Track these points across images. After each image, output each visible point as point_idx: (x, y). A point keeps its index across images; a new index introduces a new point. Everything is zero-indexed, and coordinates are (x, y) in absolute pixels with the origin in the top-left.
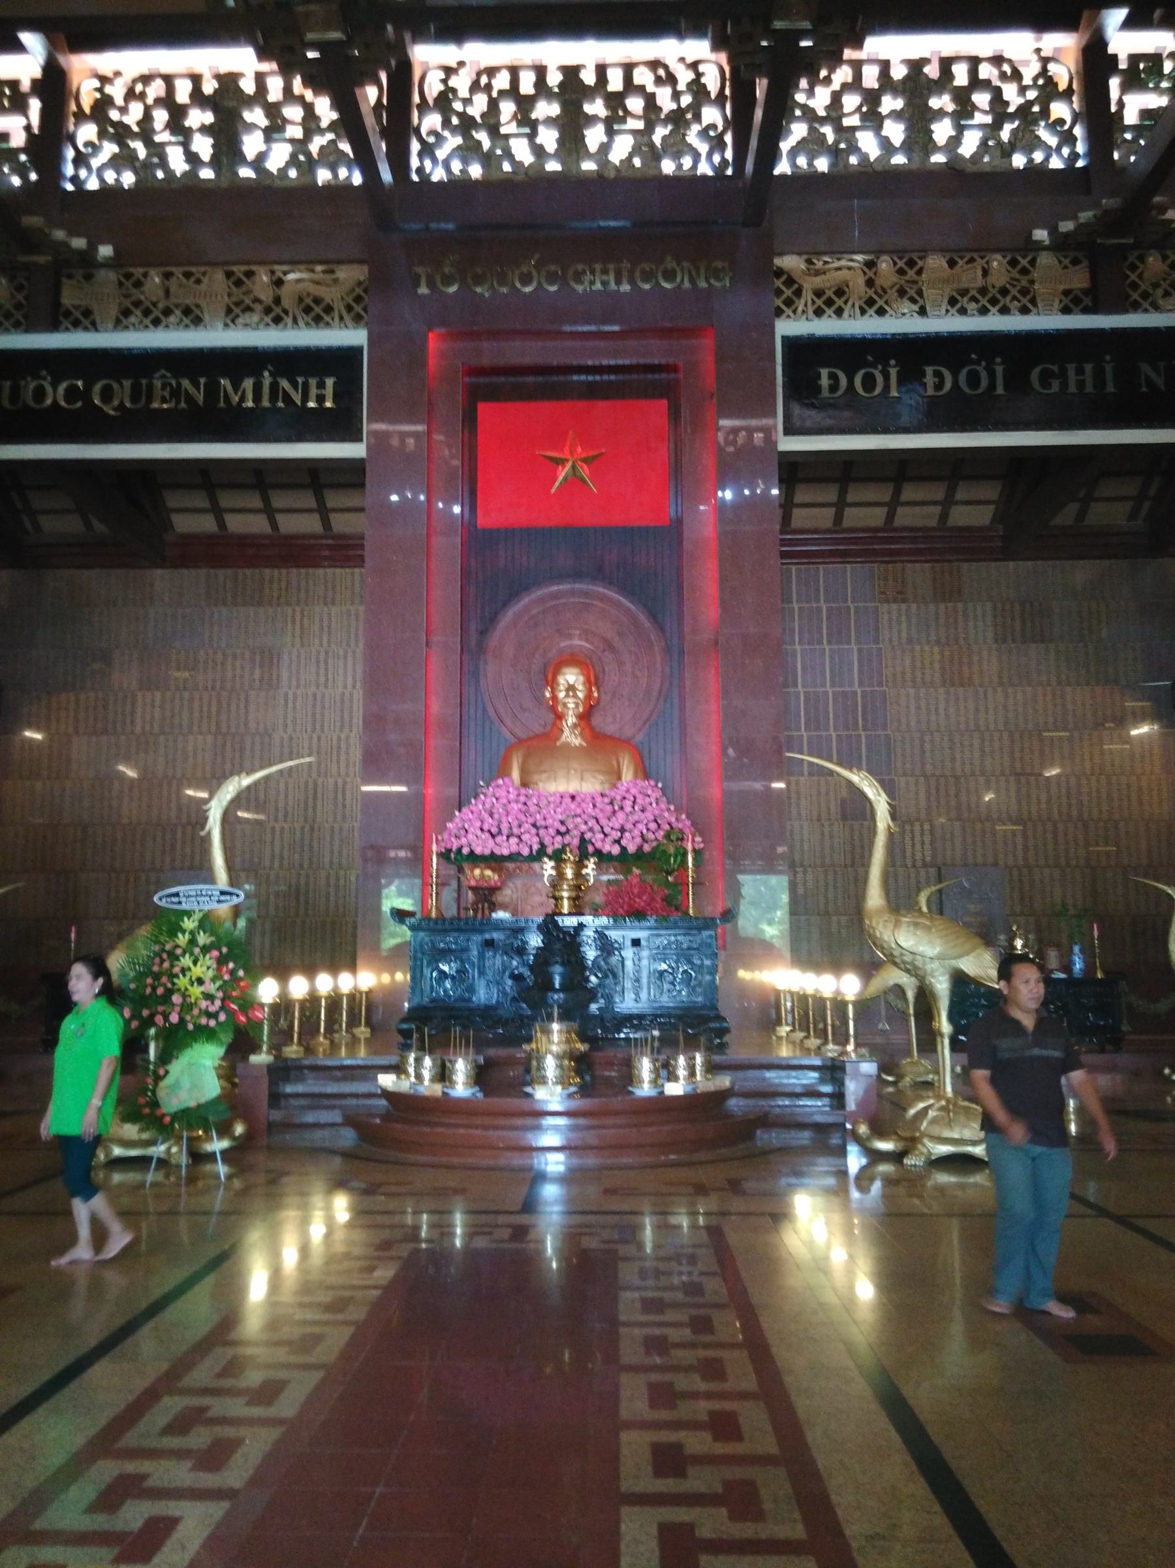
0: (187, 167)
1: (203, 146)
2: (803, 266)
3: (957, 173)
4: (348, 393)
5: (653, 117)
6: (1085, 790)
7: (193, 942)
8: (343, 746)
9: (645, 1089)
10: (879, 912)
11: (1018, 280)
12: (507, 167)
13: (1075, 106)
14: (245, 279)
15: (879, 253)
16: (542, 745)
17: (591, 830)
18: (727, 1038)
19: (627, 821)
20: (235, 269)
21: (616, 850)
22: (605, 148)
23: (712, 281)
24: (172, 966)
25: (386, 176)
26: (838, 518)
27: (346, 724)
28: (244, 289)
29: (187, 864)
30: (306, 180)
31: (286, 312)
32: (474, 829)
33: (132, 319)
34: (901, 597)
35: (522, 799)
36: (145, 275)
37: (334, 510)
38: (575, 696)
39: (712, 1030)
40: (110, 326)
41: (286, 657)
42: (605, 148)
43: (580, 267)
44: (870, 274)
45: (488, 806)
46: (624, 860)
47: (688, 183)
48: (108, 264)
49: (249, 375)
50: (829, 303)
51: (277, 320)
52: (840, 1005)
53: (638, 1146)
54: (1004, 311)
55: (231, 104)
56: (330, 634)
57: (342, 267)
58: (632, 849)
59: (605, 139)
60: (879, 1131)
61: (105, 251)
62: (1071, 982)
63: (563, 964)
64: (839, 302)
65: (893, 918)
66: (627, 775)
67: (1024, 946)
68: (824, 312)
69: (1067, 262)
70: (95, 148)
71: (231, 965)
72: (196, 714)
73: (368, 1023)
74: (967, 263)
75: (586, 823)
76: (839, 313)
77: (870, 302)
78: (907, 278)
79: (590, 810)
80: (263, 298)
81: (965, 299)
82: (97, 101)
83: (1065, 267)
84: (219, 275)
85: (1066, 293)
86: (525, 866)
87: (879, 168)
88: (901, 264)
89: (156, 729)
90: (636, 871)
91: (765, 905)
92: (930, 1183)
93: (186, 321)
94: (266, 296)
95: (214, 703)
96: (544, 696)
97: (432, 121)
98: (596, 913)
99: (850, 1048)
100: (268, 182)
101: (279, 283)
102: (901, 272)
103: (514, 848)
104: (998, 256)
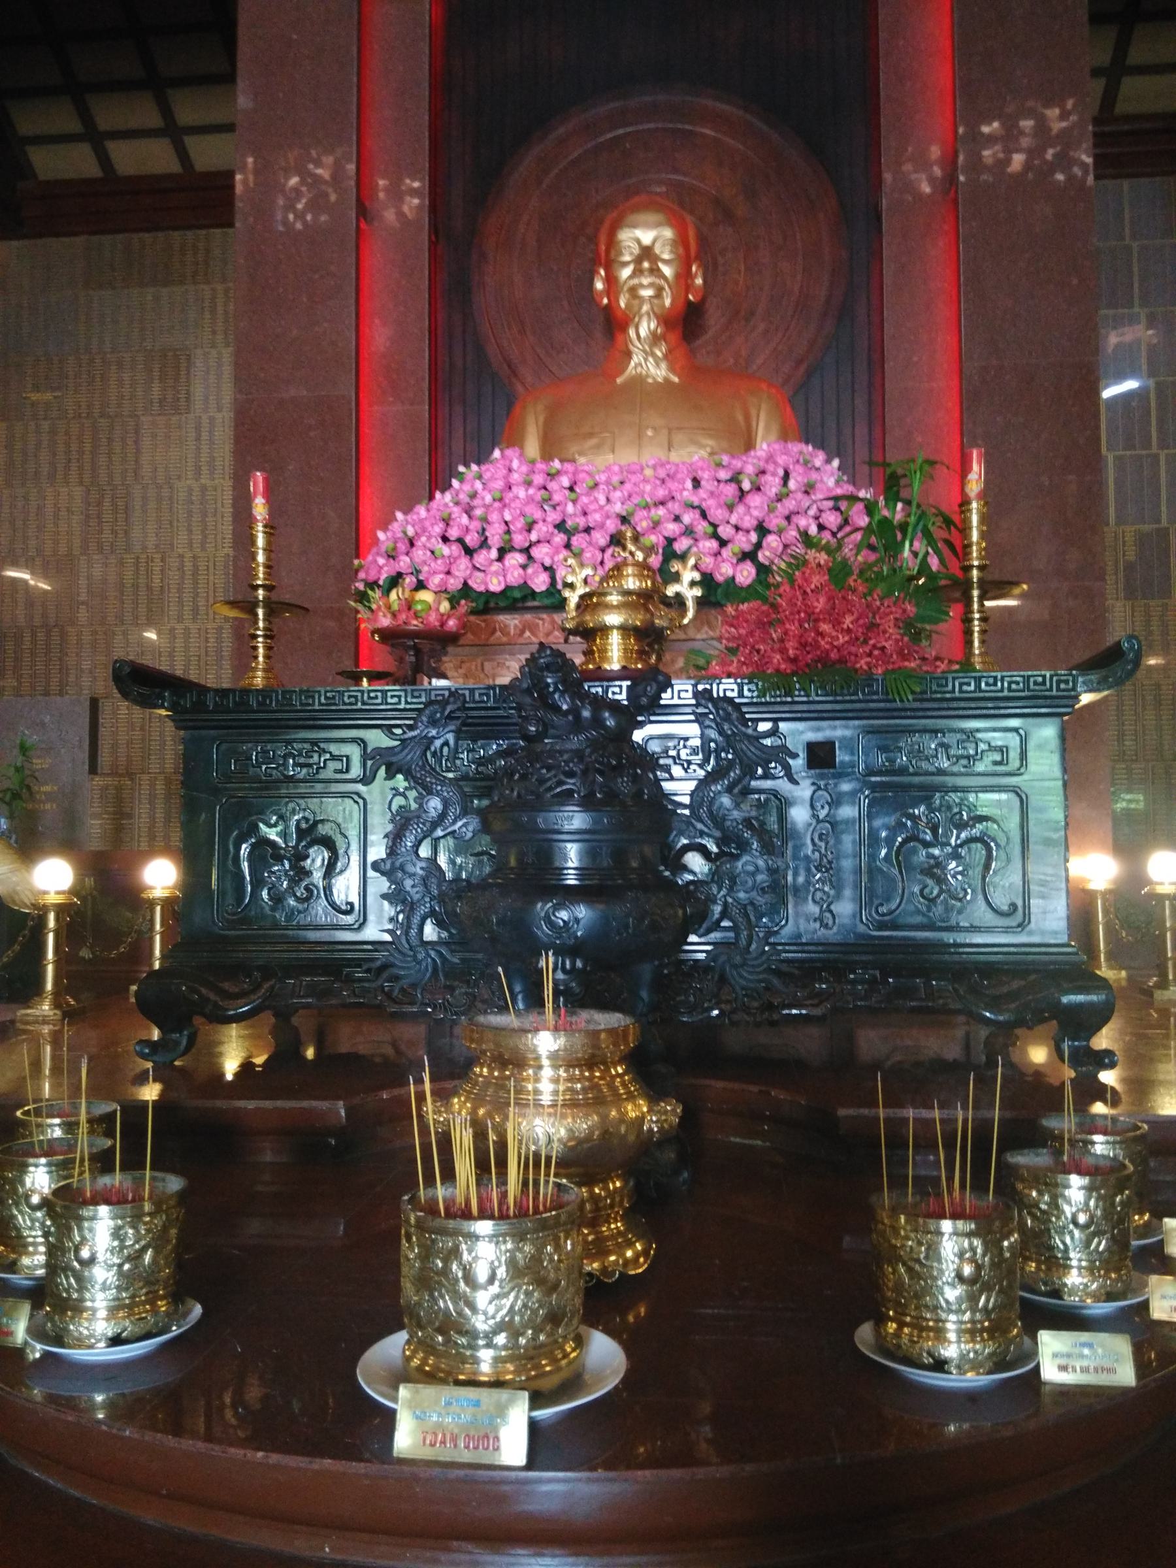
17: (689, 531)
19: (771, 510)
21: (746, 574)
38: (655, 271)
41: (199, 363)
63: (588, 803)
75: (677, 519)
79: (688, 494)
103: (515, 577)
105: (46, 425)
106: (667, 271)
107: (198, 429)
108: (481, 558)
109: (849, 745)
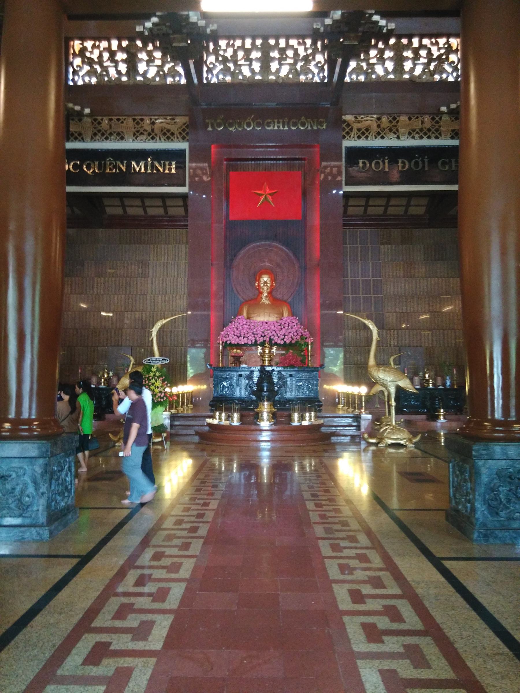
0: (117, 76)
1: (123, 68)
2: (353, 119)
3: (414, 84)
4: (181, 166)
5: (297, 58)
6: (456, 318)
7: (155, 375)
8: (174, 299)
9: (296, 423)
10: (373, 366)
11: (435, 126)
12: (240, 77)
13: (459, 56)
14: (140, 121)
15: (382, 114)
16: (254, 302)
17: (273, 335)
18: (321, 408)
20: (136, 117)
21: (282, 342)
22: (278, 71)
23: (319, 127)
24: (149, 382)
25: (196, 81)
26: (365, 211)
27: (175, 291)
28: (140, 126)
29: (117, 344)
30: (163, 82)
31: (156, 135)
32: (231, 335)
33: (97, 137)
34: (388, 242)
35: (248, 324)
36: (102, 120)
37: (169, 206)
38: (267, 285)
39: (317, 405)
40: (89, 140)
42: (278, 71)
43: (269, 121)
44: (379, 122)
45: (236, 326)
46: (285, 346)
47: (310, 85)
48: (88, 115)
49: (143, 160)
50: (363, 133)
51: (153, 138)
52: (360, 397)
53: (294, 441)
54: (429, 138)
55: (133, 51)
56: (168, 255)
57: (177, 117)
58: (288, 342)
59: (278, 67)
60: (371, 436)
61: (87, 111)
62: (445, 389)
63: (267, 383)
64: (367, 134)
65: (378, 368)
66: (286, 314)
67: (429, 376)
68: (361, 137)
69: (453, 119)
70: (81, 68)
71: (166, 382)
72: (117, 287)
73: (192, 404)
74: (416, 119)
76: (367, 137)
77: (379, 134)
78: (393, 124)
80: (147, 129)
81: (415, 133)
82: (81, 49)
83: (453, 121)
84: (130, 120)
85: (453, 131)
86: (250, 348)
87: (383, 80)
88: (390, 119)
89: (102, 292)
90: (291, 351)
91: (335, 360)
92: (386, 452)
93: (118, 138)
94: (149, 128)
95: (124, 282)
96: (255, 285)
97: (212, 59)
98: (277, 365)
99: (363, 410)
100: (148, 83)
101: (153, 123)
102: (390, 122)
103: (246, 342)
104: (427, 116)
105: (114, 279)
106: (269, 285)
107: (152, 281)
108: (240, 338)
109: (294, 375)
